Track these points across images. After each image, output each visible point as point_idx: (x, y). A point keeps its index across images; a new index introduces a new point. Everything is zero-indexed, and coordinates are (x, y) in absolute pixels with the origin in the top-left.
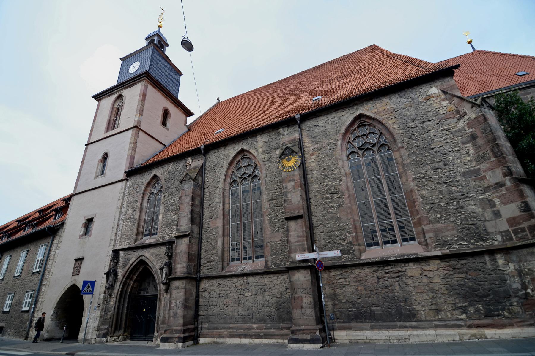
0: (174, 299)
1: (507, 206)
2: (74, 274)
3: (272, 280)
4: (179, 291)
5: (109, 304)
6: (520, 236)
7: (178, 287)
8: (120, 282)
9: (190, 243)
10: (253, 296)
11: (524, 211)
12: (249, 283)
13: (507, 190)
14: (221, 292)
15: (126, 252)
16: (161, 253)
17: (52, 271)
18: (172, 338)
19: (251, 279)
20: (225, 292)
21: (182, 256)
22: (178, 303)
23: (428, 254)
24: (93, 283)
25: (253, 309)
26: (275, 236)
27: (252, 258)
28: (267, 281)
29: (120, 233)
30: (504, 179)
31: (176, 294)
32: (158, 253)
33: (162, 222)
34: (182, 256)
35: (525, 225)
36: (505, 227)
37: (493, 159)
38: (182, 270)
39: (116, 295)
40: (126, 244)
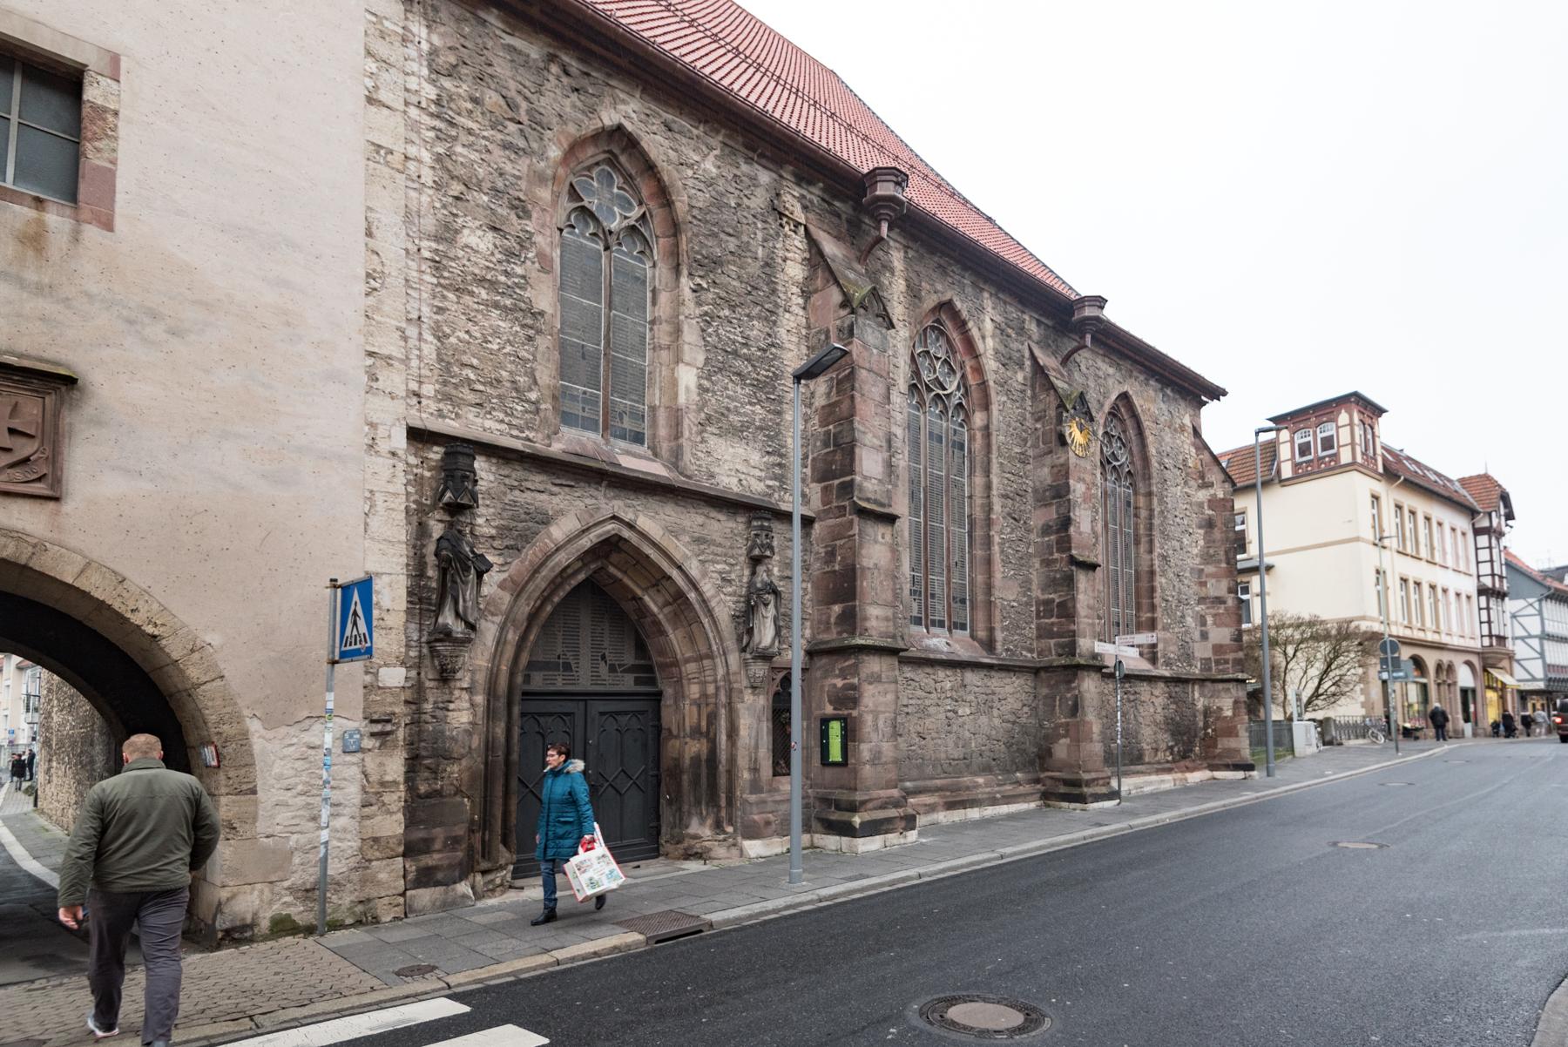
1: (1220, 629)
4: (881, 688)
6: (1221, 667)
7: (880, 677)
9: (894, 550)
11: (1235, 640)
13: (1226, 609)
14: (911, 702)
15: (517, 473)
16: (717, 537)
18: (889, 820)
20: (919, 702)
21: (881, 582)
22: (881, 724)
23: (1155, 673)
24: (365, 586)
28: (996, 684)
29: (428, 336)
30: (1227, 595)
33: (701, 409)
34: (881, 582)
35: (1231, 656)
36: (1209, 654)
37: (1224, 565)
39: (481, 678)
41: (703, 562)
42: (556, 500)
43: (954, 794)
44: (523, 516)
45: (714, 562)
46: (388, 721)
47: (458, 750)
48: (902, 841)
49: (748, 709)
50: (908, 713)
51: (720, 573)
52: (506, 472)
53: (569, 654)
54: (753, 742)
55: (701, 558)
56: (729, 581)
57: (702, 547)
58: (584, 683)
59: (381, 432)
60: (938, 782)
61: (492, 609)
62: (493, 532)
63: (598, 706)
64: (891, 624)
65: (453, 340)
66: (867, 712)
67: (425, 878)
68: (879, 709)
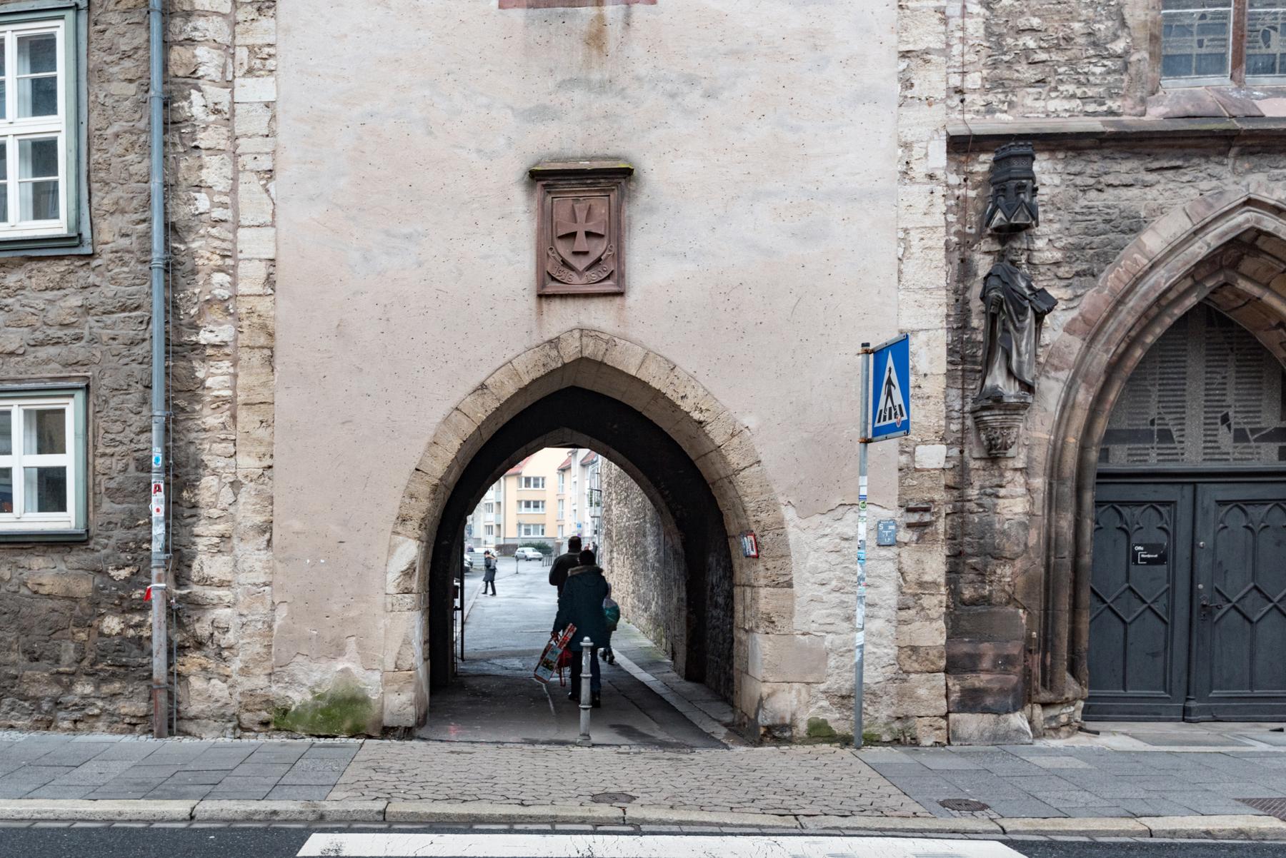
2: (552, 287)
8: (1064, 375)
15: (1092, 166)
17: (253, 244)
39: (1041, 454)
40: (1055, 104)
42: (1151, 193)
44: (1101, 226)
46: (926, 510)
47: (1010, 548)
52: (1072, 170)
53: (1168, 417)
58: (1192, 456)
59: (917, 152)
61: (1056, 362)
62: (1058, 255)
67: (971, 701)
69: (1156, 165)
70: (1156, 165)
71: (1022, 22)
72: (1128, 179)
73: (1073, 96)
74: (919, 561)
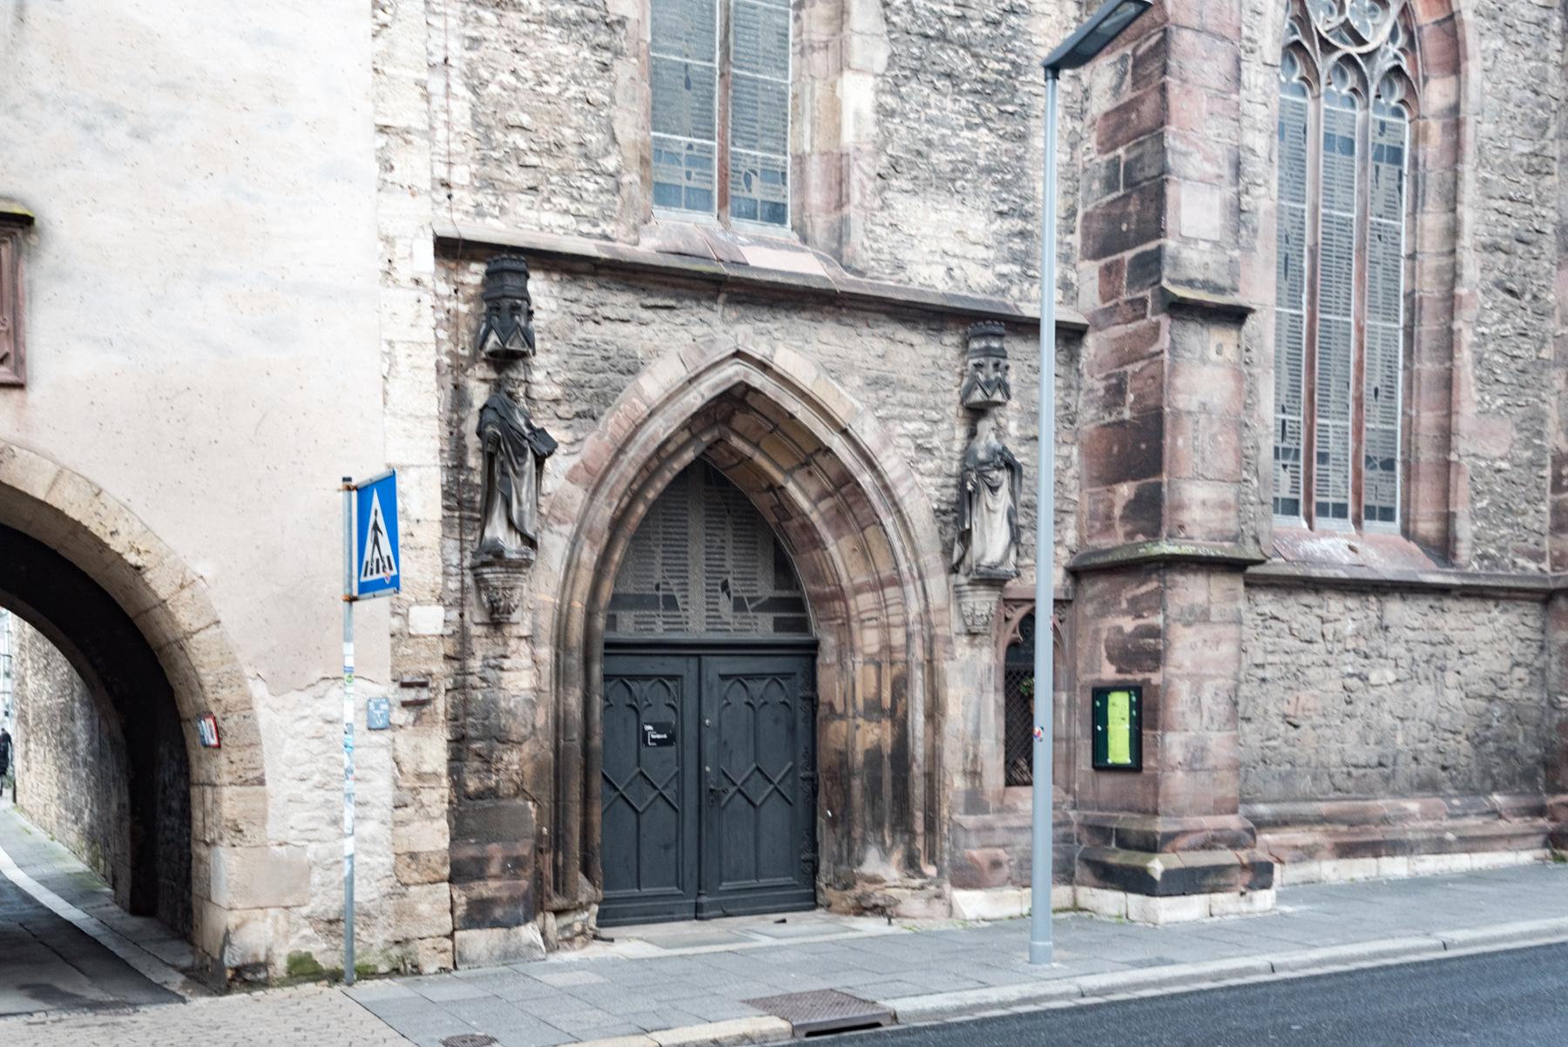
0: (1189, 676)
3: (1468, 624)
4: (1207, 632)
5: (497, 685)
8: (568, 529)
10: (1398, 687)
12: (1386, 628)
14: (1270, 658)
15: (589, 294)
18: (1220, 870)
19: (1397, 610)
20: (1288, 659)
21: (1213, 437)
22: (1207, 697)
25: (1400, 739)
26: (1492, 433)
27: (1302, 509)
28: (1453, 624)
29: (459, 89)
31: (1193, 647)
32: (877, 368)
33: (880, 149)
34: (1213, 437)
38: (1215, 519)
39: (547, 621)
41: (883, 420)
42: (647, 332)
43: (1356, 829)
44: (600, 364)
45: (902, 419)
46: (424, 685)
47: (517, 730)
48: (1244, 907)
49: (962, 671)
50: (1264, 680)
51: (914, 437)
52: (569, 295)
53: (672, 582)
54: (970, 727)
55: (881, 413)
56: (929, 451)
57: (882, 394)
58: (696, 627)
59: (400, 250)
60: (1324, 808)
61: (559, 514)
63: (717, 666)
64: (1232, 513)
65: (493, 88)
66: (1180, 677)
67: (479, 915)
68: (1205, 671)
69: (650, 302)
70: (650, 302)
71: (512, 117)
72: (624, 314)
73: (567, 212)
74: (416, 748)
